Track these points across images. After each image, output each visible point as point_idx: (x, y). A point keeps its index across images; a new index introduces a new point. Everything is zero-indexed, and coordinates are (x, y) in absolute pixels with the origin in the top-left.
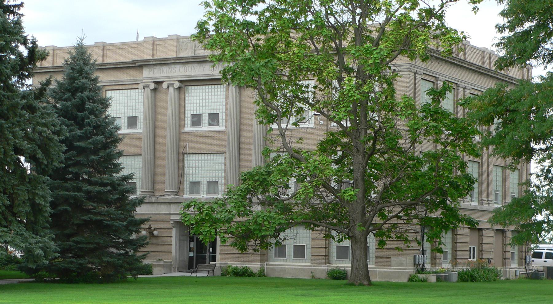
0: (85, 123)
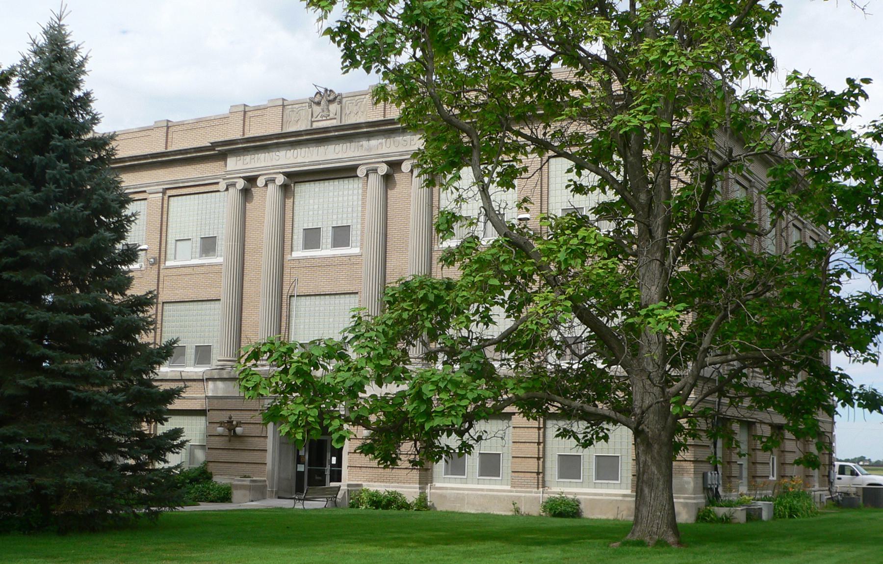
0: (47, 176)
